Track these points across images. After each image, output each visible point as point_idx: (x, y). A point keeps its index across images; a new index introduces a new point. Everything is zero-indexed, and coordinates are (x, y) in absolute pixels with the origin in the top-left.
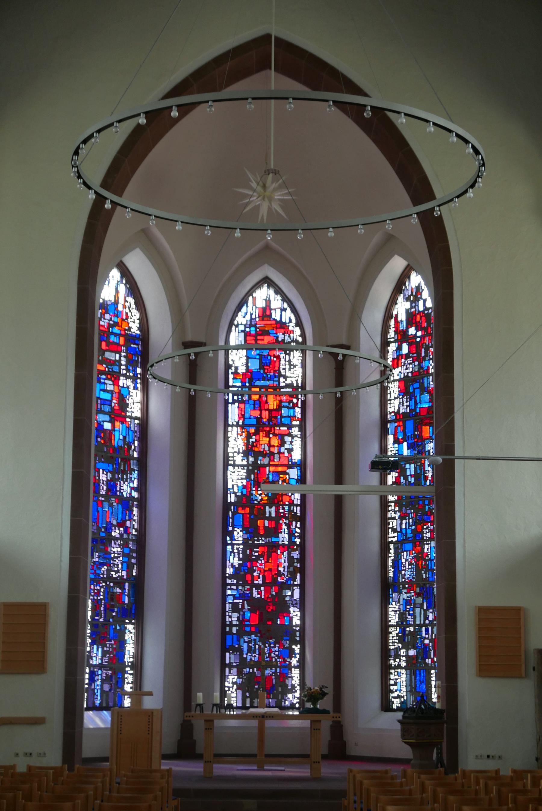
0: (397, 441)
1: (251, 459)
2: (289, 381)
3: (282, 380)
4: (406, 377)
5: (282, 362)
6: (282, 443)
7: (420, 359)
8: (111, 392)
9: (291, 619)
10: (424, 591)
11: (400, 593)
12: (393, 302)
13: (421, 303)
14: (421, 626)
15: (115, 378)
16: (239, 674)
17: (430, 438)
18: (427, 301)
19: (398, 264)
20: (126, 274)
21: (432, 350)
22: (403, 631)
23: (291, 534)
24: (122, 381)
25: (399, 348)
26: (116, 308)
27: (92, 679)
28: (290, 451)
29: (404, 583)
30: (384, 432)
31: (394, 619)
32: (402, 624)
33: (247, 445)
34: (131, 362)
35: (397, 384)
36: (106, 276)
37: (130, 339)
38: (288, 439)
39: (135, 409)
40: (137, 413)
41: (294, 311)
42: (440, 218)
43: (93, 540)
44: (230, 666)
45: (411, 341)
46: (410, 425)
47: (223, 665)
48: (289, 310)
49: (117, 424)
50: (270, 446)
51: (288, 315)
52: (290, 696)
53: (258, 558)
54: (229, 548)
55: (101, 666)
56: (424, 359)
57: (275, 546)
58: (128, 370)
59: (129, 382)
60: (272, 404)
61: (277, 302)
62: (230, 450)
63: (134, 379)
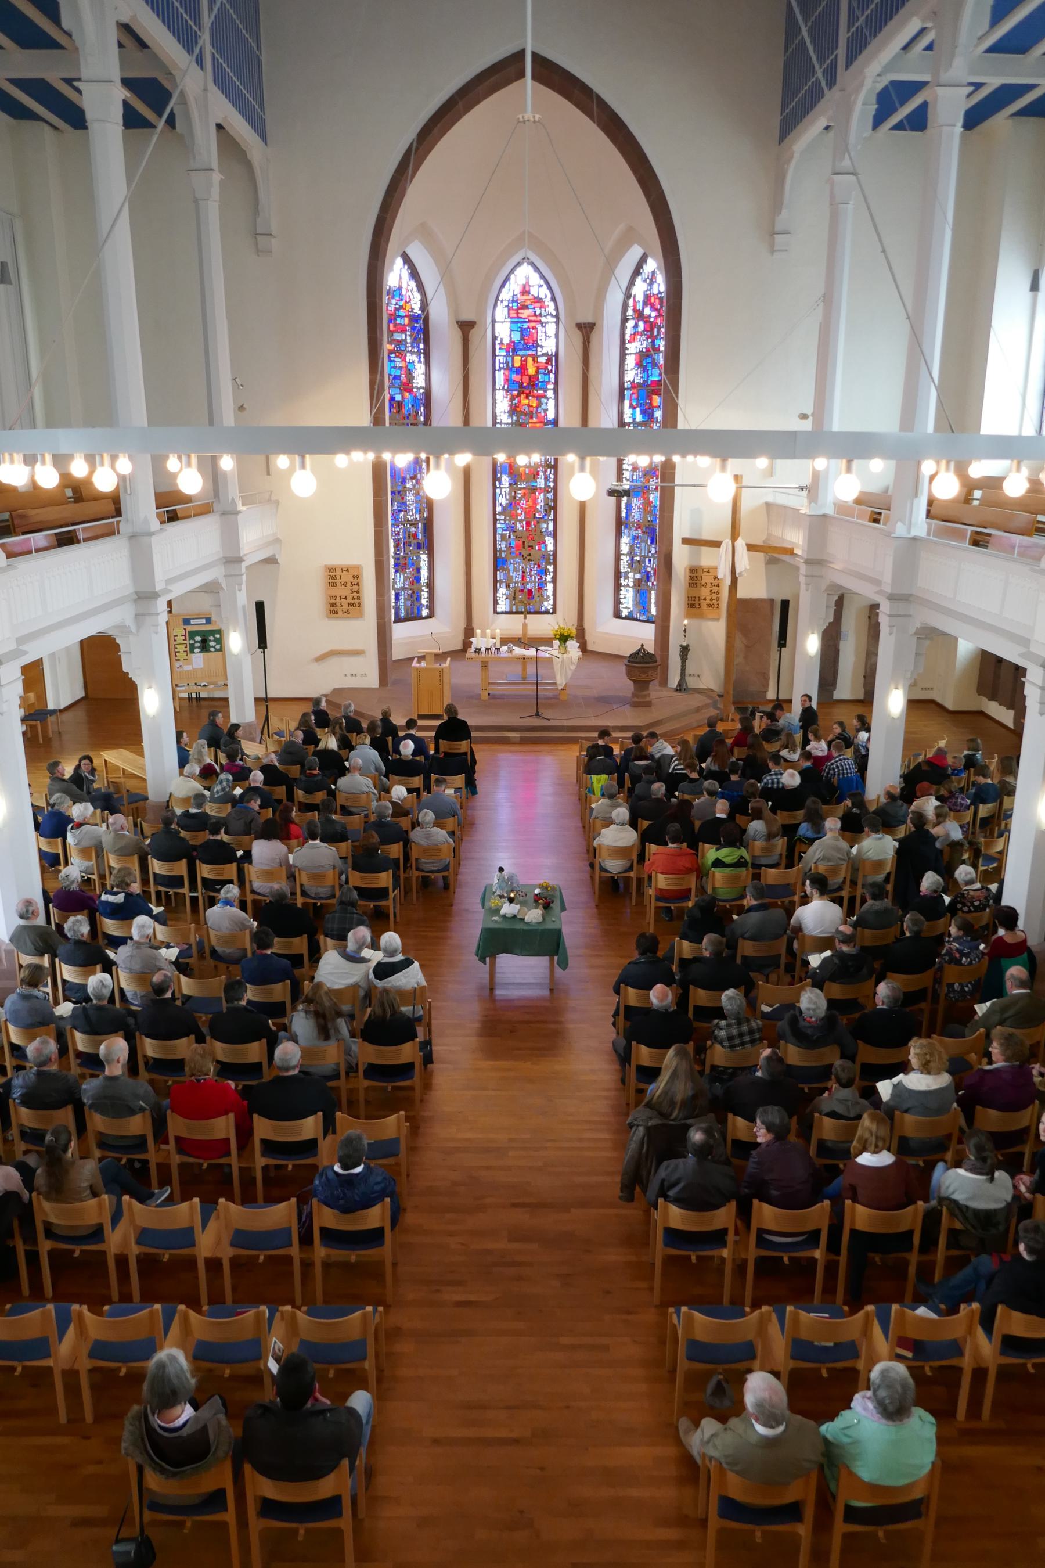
0: (632, 406)
1: (515, 418)
2: (545, 351)
3: (539, 349)
4: (641, 351)
5: (539, 333)
6: (539, 405)
7: (654, 338)
8: (400, 368)
9: (546, 546)
10: (650, 532)
11: (630, 529)
12: (632, 283)
13: (655, 286)
14: (645, 557)
15: (401, 354)
16: (508, 586)
17: (659, 407)
18: (660, 286)
19: (635, 252)
20: (407, 260)
21: (663, 330)
22: (632, 559)
23: (547, 479)
24: (409, 357)
25: (636, 326)
26: (401, 294)
27: (397, 598)
28: (546, 410)
29: (633, 523)
30: (622, 397)
31: (625, 549)
32: (631, 554)
33: (511, 405)
34: (415, 340)
35: (633, 356)
36: (393, 263)
37: (414, 319)
38: (544, 401)
39: (419, 381)
40: (422, 384)
41: (549, 288)
42: (800, 721)
43: (393, 493)
44: (501, 581)
45: (646, 319)
46: (643, 393)
47: (495, 581)
48: (545, 287)
49: (407, 395)
50: (529, 406)
51: (544, 293)
52: (546, 603)
53: (521, 499)
54: (498, 491)
55: (404, 588)
56: (656, 337)
57: (534, 490)
58: (413, 347)
59: (414, 358)
60: (531, 371)
61: (535, 279)
62: (497, 411)
63: (418, 354)
